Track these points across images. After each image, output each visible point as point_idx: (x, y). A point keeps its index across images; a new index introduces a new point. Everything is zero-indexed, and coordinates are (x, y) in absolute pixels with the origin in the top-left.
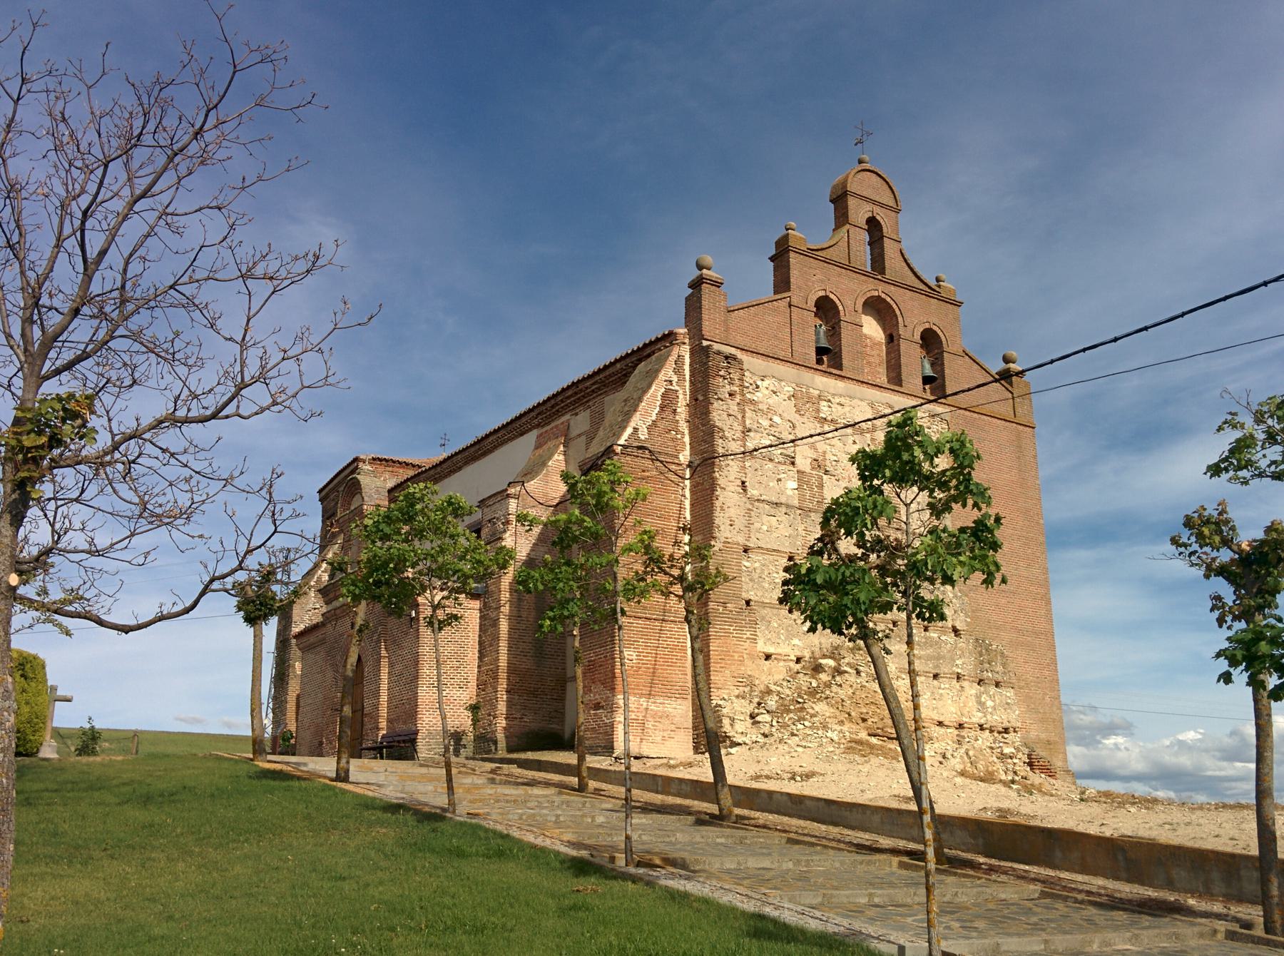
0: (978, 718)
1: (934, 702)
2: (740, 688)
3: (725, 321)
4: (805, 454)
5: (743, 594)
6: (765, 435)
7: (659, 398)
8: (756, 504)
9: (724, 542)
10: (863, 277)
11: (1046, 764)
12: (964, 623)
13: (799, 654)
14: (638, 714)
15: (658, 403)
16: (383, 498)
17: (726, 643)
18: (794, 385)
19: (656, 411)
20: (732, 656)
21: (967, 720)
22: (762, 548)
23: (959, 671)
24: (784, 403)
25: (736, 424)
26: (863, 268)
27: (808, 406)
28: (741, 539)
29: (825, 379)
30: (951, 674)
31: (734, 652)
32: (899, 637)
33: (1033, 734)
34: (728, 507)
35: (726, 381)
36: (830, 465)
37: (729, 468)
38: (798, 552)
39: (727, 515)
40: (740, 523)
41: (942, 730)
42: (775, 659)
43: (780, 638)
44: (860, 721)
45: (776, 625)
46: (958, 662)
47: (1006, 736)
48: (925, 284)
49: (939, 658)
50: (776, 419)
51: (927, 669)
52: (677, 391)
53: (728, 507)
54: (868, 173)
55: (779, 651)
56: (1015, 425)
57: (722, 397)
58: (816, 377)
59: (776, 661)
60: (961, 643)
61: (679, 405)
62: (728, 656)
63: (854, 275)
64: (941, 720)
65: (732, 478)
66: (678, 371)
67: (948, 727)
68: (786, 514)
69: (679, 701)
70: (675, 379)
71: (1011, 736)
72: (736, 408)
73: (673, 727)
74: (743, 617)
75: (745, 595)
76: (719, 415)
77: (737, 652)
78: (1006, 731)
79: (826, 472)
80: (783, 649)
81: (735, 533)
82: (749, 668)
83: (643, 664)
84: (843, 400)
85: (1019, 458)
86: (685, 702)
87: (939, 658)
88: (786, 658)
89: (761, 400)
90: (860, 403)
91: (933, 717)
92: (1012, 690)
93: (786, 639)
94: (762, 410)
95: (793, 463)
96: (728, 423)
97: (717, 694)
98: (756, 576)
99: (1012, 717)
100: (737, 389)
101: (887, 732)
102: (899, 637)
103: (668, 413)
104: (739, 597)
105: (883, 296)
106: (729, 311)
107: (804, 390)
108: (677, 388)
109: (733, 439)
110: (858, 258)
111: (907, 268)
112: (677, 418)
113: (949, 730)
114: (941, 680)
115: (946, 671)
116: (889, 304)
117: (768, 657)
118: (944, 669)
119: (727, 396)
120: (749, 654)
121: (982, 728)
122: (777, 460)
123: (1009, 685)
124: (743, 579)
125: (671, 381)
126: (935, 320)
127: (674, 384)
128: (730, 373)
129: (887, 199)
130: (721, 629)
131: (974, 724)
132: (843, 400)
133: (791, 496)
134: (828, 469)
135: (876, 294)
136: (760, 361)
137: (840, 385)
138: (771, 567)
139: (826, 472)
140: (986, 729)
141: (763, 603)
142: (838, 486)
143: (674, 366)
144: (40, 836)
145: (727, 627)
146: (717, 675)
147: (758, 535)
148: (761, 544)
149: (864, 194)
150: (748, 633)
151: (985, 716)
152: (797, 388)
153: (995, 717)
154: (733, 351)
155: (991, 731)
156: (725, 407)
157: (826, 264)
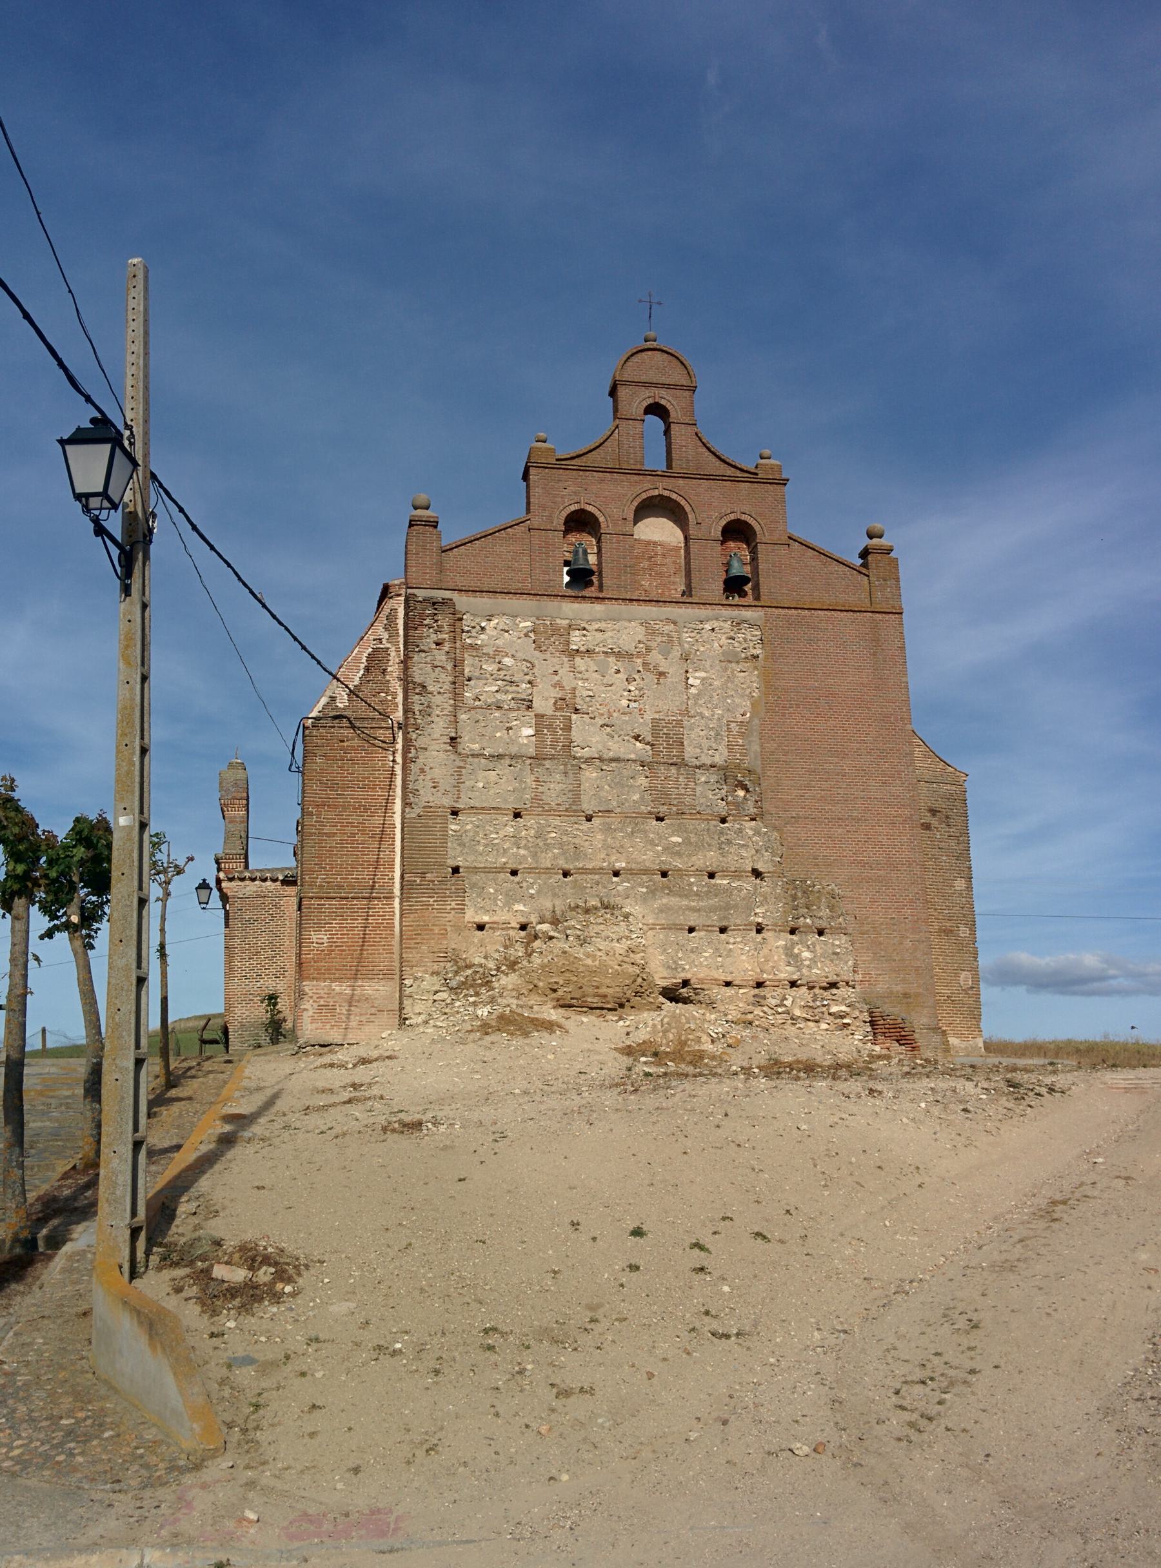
0: (786, 972)
1: (720, 959)
2: (441, 964)
3: (441, 564)
4: (546, 694)
5: (449, 861)
6: (490, 681)
7: (364, 660)
8: (470, 759)
9: (424, 807)
10: (636, 477)
11: (899, 1021)
12: (770, 864)
13: (523, 920)
14: (329, 1000)
15: (363, 666)
16: (241, 790)
17: (424, 916)
18: (533, 619)
19: (360, 675)
20: (431, 930)
21: (770, 977)
22: (476, 808)
23: (760, 920)
24: (519, 641)
25: (443, 676)
26: (639, 467)
27: (552, 639)
28: (447, 802)
29: (576, 606)
30: (745, 925)
31: (433, 925)
32: (669, 888)
33: (881, 987)
34: (431, 768)
35: (431, 630)
36: (581, 702)
37: (433, 725)
38: (526, 806)
39: (428, 777)
40: (446, 783)
41: (729, 991)
42: (490, 928)
43: (497, 905)
44: (548, 992)
45: (492, 891)
46: (757, 911)
47: (834, 991)
48: (742, 470)
49: (727, 907)
50: (507, 661)
51: (709, 923)
52: (388, 649)
53: (431, 768)
54: (650, 353)
55: (495, 919)
56: (870, 614)
57: (426, 649)
58: (564, 604)
59: (491, 931)
60: (765, 886)
61: (391, 663)
62: (426, 930)
63: (623, 477)
64: (729, 979)
65: (436, 736)
66: (390, 626)
67: (740, 987)
68: (510, 766)
69: (383, 982)
70: (385, 636)
71: (842, 992)
72: (444, 658)
73: (373, 1010)
74: (448, 887)
75: (452, 863)
76: (421, 669)
77: (439, 925)
78: (833, 985)
79: (576, 711)
80: (502, 916)
81: (440, 794)
82: (453, 942)
83: (336, 946)
84: (602, 625)
85: (875, 654)
86: (391, 983)
87: (727, 907)
88: (505, 926)
89: (485, 642)
90: (627, 624)
91: (716, 976)
92: (844, 937)
93: (505, 906)
94: (488, 654)
95: (529, 707)
96: (433, 675)
97: (411, 972)
98: (466, 839)
99: (844, 970)
100: (446, 636)
101: (586, 1002)
102: (669, 888)
103: (375, 675)
104: (443, 865)
105: (666, 493)
106: (443, 552)
107: (548, 623)
108: (388, 645)
109: (439, 693)
110: (632, 456)
111: (707, 453)
112: (388, 677)
113: (741, 991)
114: (730, 933)
115: (738, 922)
116: (676, 501)
117: (481, 927)
118: (735, 919)
119: (434, 646)
120: (454, 926)
121: (793, 984)
122: (506, 707)
123: (840, 931)
124: (449, 844)
125: (380, 639)
126: (746, 509)
127: (384, 641)
128: (436, 621)
129: (677, 376)
130: (416, 902)
131: (780, 981)
132: (602, 625)
133: (526, 744)
134: (579, 707)
135: (656, 493)
136: (485, 600)
137: (599, 608)
138: (488, 827)
139: (576, 711)
140: (801, 985)
141: (476, 868)
142: (593, 725)
143: (385, 622)
144: (742, 1068)
145: (424, 899)
146: (411, 952)
147: (470, 794)
148: (472, 803)
149: (643, 378)
150: (453, 903)
151: (798, 971)
152: (538, 622)
153: (814, 971)
154: (447, 594)
155: (811, 988)
156: (428, 659)
157: (581, 473)
